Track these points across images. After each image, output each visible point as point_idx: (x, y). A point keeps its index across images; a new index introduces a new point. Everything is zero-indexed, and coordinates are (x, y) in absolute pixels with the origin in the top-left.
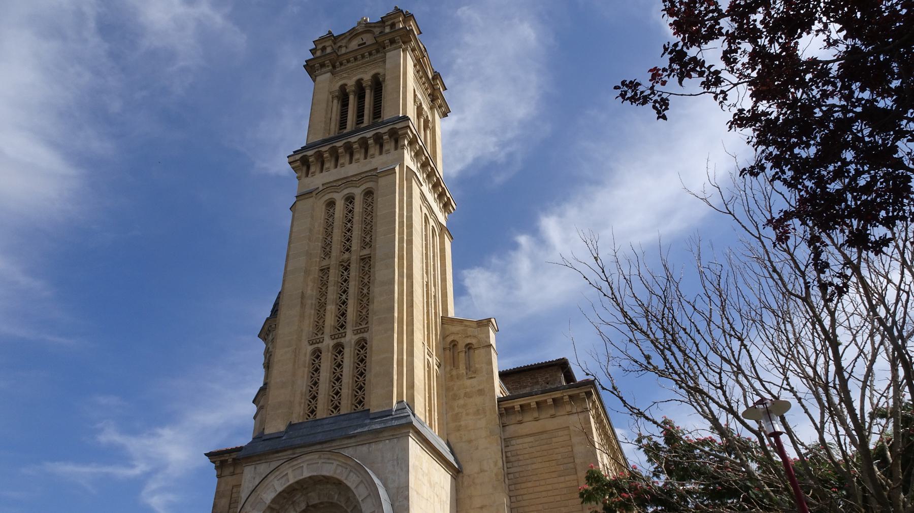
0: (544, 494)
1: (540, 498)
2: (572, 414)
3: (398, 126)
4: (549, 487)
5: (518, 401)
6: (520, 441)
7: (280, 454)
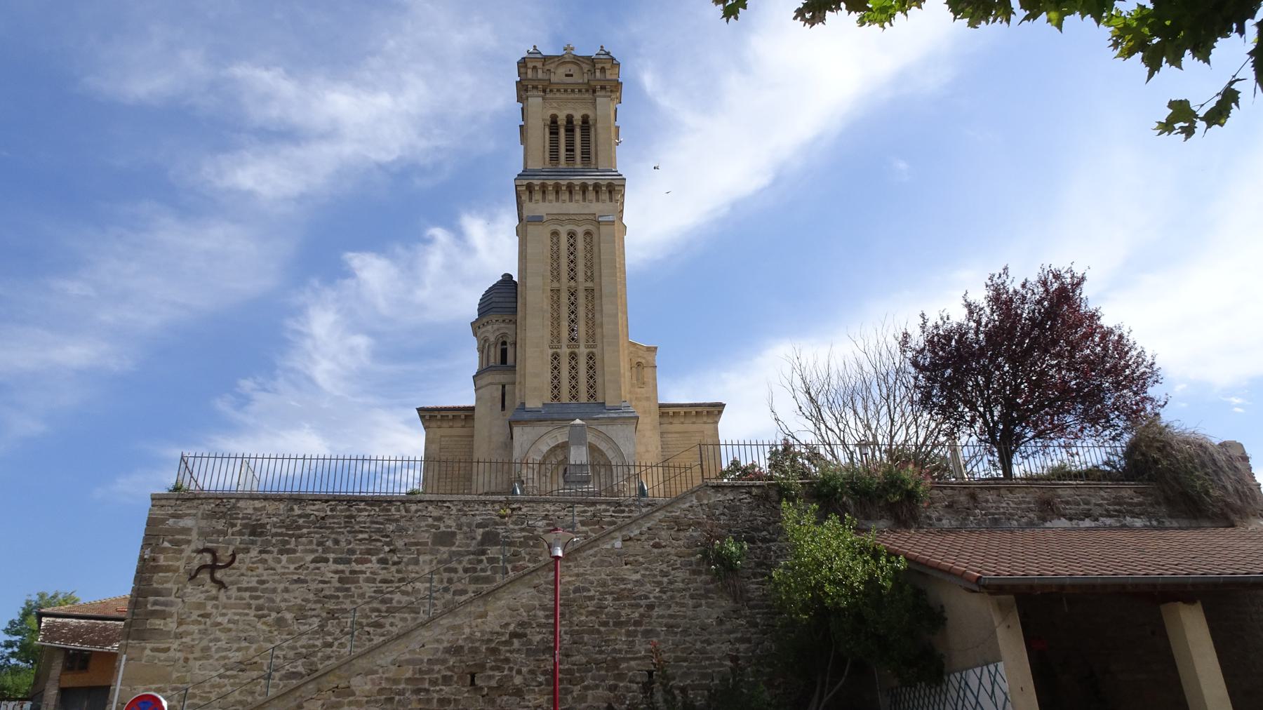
3: (616, 182)
6: (669, 435)
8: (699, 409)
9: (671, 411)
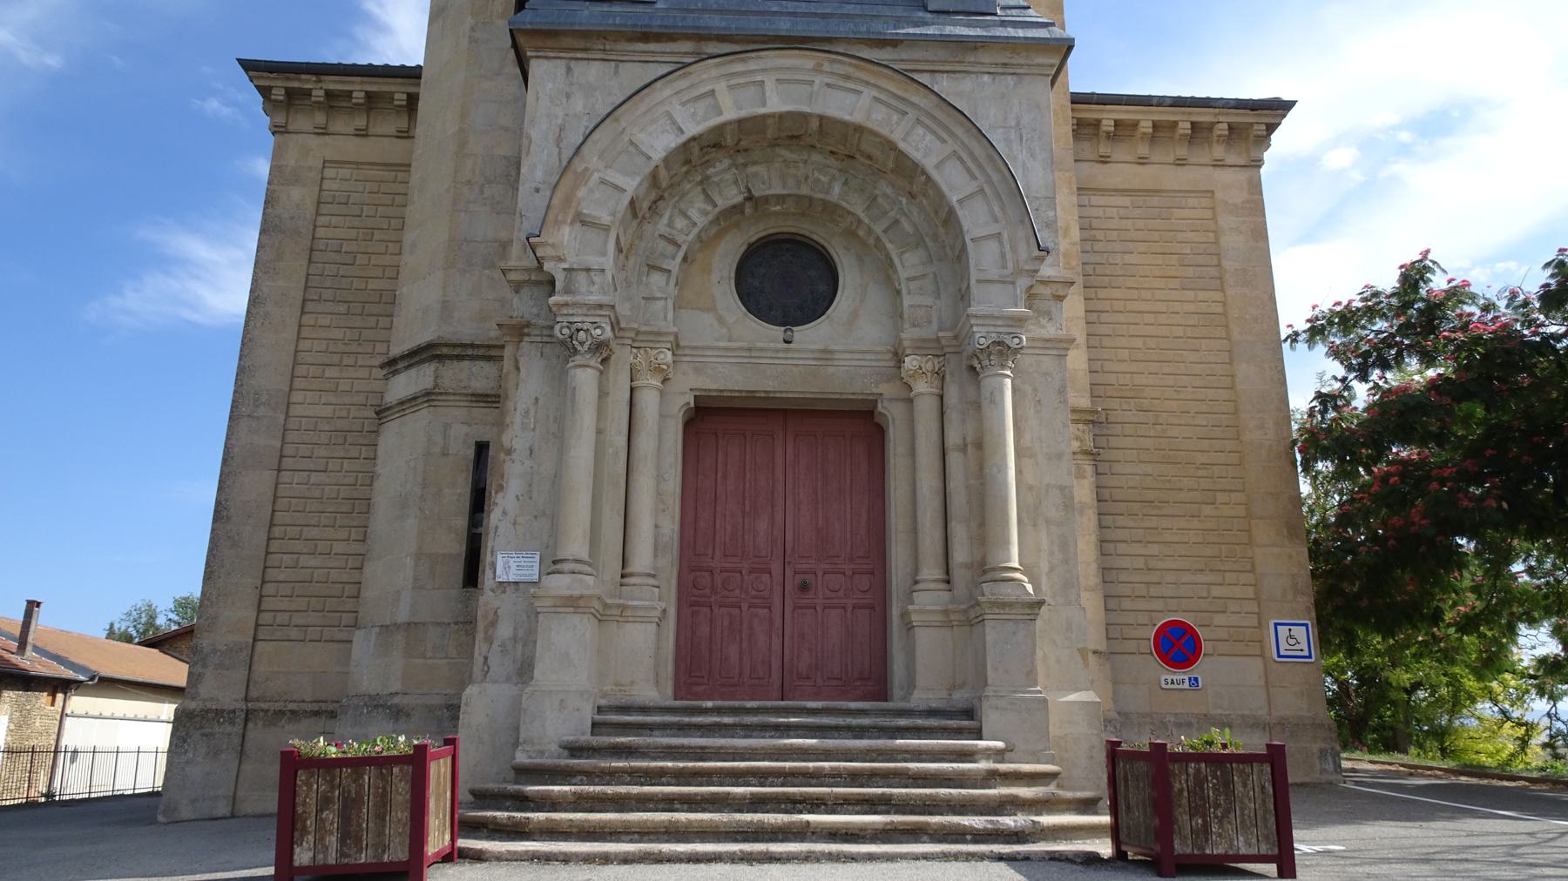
0: (1149, 318)
1: (1137, 324)
2: (1223, 166)
4: (1161, 307)
5: (1113, 111)
7: (652, 46)
8: (1204, 116)
9: (1108, 116)
